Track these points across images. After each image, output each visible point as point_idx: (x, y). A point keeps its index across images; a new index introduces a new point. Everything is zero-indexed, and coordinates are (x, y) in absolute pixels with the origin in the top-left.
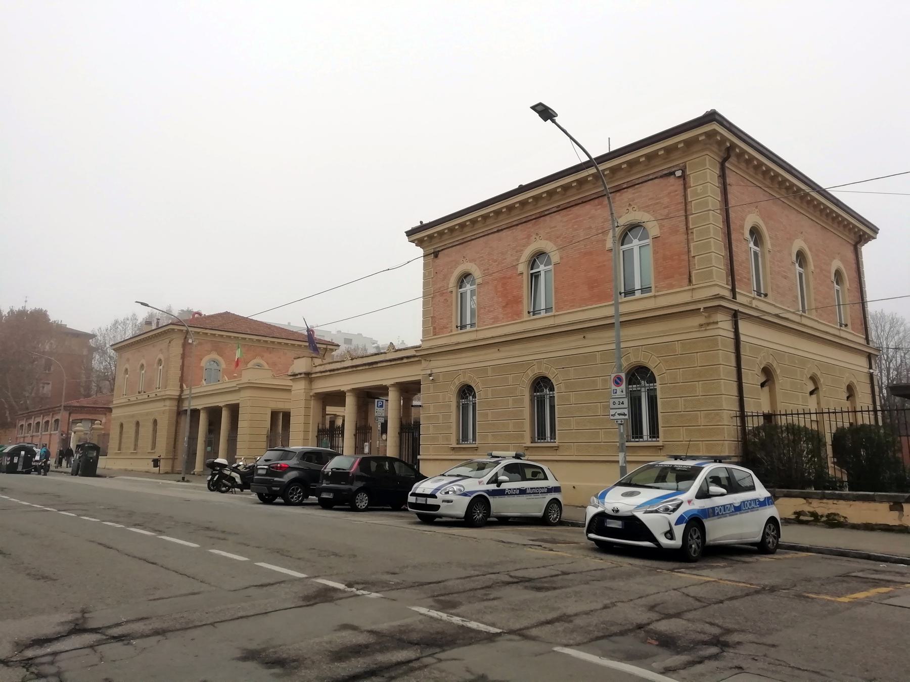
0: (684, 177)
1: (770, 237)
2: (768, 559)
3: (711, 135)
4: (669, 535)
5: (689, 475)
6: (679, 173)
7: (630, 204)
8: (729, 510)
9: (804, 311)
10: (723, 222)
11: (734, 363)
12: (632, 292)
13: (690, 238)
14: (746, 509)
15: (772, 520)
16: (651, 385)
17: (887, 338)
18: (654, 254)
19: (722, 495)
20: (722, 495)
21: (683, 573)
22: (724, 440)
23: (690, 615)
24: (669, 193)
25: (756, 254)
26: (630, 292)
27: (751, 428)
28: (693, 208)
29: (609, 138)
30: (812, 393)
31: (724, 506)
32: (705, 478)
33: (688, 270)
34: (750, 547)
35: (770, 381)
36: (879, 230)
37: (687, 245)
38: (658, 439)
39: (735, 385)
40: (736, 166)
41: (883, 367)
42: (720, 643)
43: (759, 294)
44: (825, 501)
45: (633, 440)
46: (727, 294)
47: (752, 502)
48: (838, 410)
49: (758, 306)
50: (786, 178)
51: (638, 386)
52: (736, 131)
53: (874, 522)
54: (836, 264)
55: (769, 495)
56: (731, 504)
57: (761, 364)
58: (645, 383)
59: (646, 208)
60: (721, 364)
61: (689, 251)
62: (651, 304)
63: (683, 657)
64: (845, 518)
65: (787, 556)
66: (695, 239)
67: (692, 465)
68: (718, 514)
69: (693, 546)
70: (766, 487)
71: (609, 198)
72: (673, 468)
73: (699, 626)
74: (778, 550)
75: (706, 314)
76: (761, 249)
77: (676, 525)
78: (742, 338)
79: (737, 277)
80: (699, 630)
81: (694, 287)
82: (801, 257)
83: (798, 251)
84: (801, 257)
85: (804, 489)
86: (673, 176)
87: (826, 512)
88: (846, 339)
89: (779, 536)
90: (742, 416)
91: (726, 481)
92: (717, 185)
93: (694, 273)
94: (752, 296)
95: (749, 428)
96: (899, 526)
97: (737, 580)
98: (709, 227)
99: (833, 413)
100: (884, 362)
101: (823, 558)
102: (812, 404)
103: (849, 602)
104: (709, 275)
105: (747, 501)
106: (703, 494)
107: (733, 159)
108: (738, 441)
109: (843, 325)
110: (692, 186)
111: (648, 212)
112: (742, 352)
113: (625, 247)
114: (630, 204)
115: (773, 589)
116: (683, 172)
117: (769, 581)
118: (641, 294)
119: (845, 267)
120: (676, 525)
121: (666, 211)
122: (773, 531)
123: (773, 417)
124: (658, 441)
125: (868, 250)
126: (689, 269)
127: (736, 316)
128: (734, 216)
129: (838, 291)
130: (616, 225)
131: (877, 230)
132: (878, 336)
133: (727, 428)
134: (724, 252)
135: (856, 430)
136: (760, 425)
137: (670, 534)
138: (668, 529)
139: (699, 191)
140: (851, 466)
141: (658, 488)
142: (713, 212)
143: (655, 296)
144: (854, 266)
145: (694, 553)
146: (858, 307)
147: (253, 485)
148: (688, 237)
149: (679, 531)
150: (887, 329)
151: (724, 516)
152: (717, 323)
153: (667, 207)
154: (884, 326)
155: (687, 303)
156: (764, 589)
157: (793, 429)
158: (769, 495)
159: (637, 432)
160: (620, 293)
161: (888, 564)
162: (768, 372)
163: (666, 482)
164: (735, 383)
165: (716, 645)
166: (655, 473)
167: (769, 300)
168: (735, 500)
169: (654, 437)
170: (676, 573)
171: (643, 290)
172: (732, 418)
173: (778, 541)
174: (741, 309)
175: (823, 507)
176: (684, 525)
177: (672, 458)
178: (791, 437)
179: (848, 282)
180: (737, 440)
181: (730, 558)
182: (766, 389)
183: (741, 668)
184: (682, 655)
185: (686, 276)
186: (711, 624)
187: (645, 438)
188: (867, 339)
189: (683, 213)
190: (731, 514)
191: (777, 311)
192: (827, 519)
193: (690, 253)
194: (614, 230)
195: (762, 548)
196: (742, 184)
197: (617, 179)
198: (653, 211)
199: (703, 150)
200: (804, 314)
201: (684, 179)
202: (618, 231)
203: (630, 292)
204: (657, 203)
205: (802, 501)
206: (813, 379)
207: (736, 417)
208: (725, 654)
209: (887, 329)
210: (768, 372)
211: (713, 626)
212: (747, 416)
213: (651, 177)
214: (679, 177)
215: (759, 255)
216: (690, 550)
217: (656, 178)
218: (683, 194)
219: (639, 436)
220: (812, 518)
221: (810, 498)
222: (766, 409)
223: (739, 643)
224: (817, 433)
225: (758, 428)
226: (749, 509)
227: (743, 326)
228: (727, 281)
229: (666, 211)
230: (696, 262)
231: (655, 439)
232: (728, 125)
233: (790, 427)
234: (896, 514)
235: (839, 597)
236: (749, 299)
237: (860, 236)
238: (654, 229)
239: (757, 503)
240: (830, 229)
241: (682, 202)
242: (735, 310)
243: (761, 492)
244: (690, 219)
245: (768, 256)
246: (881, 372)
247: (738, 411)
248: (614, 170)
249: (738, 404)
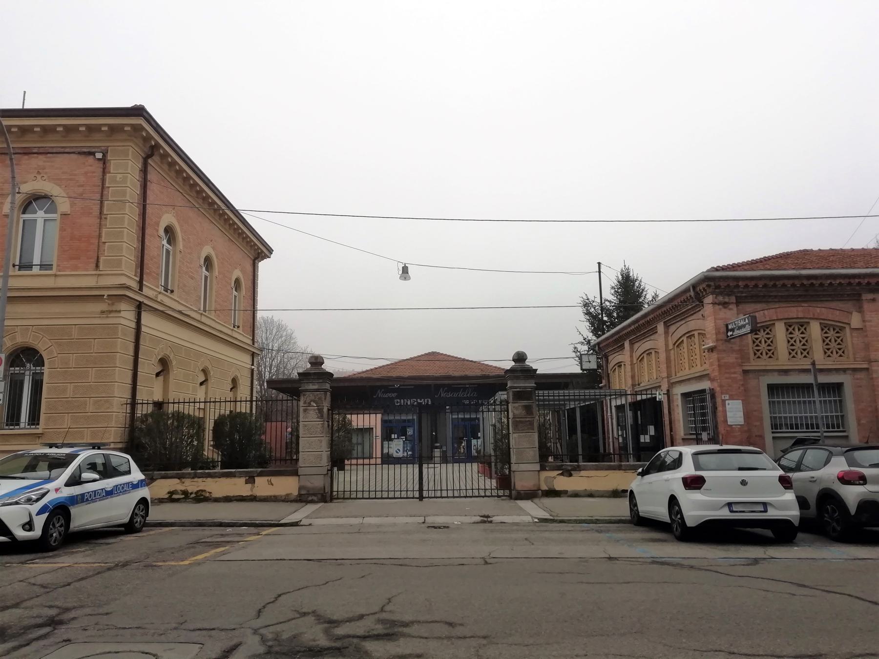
0: (104, 160)
1: (183, 239)
2: (132, 538)
3: (137, 129)
4: (27, 526)
5: (61, 463)
6: (99, 156)
7: (38, 171)
8: (100, 495)
9: (205, 311)
10: (139, 215)
11: (132, 352)
12: (29, 267)
13: (103, 223)
14: (118, 493)
15: (143, 501)
16: (37, 368)
17: (273, 340)
18: (60, 230)
19: (94, 480)
20: (94, 480)
21: (37, 563)
22: (107, 427)
23: (29, 604)
24: (86, 173)
25: (168, 252)
26: (25, 266)
27: (140, 415)
28: (110, 193)
29: (25, 92)
30: (201, 384)
31: (95, 491)
32: (79, 465)
33: (96, 255)
34: (111, 529)
35: (165, 372)
36: (273, 251)
37: (98, 230)
38: (37, 426)
39: (130, 374)
40: (159, 165)
41: (267, 364)
42: (54, 623)
43: (166, 290)
44: (196, 480)
45: (7, 427)
46: (134, 285)
47: (125, 485)
48: (223, 399)
49: (164, 301)
50: (203, 189)
51: (22, 368)
52: (162, 133)
53: (232, 495)
54: (237, 273)
55: (143, 477)
56: (102, 489)
57: (158, 354)
58: (30, 367)
59: (57, 181)
60: (118, 352)
61: (100, 236)
62: (49, 283)
63: (9, 644)
64: (210, 493)
65: (151, 533)
66: (108, 225)
67: (67, 453)
68: (87, 500)
69: (54, 535)
70: (141, 471)
71: (11, 159)
72: (45, 456)
73: (35, 612)
74: (144, 529)
75: (110, 302)
76: (173, 248)
77: (36, 515)
78: (143, 329)
79: (146, 271)
80: (35, 615)
81: (101, 272)
82: (208, 262)
83: (206, 257)
84: (208, 262)
85: (181, 471)
86: (92, 156)
87: (195, 489)
88: (236, 339)
89: (147, 514)
90: (133, 404)
91: (102, 466)
92: (138, 179)
93: (102, 259)
94: (159, 290)
95: (138, 415)
96: (251, 496)
97: (93, 561)
98: (124, 217)
99: (213, 402)
100: (268, 360)
101: (183, 530)
102: (200, 395)
103: (190, 564)
104: (119, 264)
105: (121, 485)
106: (74, 481)
107: (156, 158)
108: (125, 428)
109: (236, 327)
110: (111, 172)
111: (60, 186)
112: (142, 342)
113: (27, 216)
114: (38, 171)
115: (125, 564)
116: (104, 155)
117: (123, 558)
118: (40, 270)
119: (244, 277)
120: (36, 515)
121: (81, 190)
122: (142, 512)
123: (165, 405)
124: (38, 428)
125: (262, 265)
126: (98, 254)
127: (140, 307)
128: (151, 212)
129: (235, 296)
130: (17, 191)
131: (271, 251)
132: (267, 338)
133: (116, 415)
134: (136, 244)
135: (234, 417)
136: (149, 412)
137: (29, 526)
138: (27, 520)
139: (118, 179)
140: (225, 448)
141: (23, 478)
142: (131, 204)
143: (56, 276)
144: (251, 277)
145: (55, 542)
146: (250, 313)
147: (650, 374)
148: (100, 221)
149: (39, 522)
150: (274, 332)
151: (93, 501)
152: (120, 311)
153: (82, 186)
154: (272, 330)
155: (91, 288)
156: (117, 565)
157: (179, 417)
158: (143, 477)
159: (13, 418)
160: (14, 266)
161: (235, 528)
162: (164, 363)
163: (36, 471)
164: (131, 371)
165: (49, 625)
166: (25, 462)
167: (175, 296)
168: (108, 484)
169: (33, 424)
170: (27, 565)
171: (42, 266)
172: (122, 405)
173: (145, 520)
174: (146, 302)
175: (192, 486)
176: (46, 515)
177: (45, 446)
178: (176, 424)
179: (244, 292)
180: (124, 426)
181: (94, 541)
182: (161, 378)
183: (69, 640)
184: (9, 643)
185: (94, 260)
186: (50, 607)
187: (22, 425)
188: (253, 340)
189: (98, 196)
190: (102, 498)
191: (180, 308)
192: (195, 495)
193: (101, 238)
194: (14, 195)
195: (129, 528)
196: (163, 184)
197: (27, 141)
198: (66, 187)
199: (126, 140)
200: (204, 313)
201: (104, 163)
202: (19, 198)
203: (25, 266)
204: (71, 180)
205: (177, 481)
206: (205, 371)
207: (127, 404)
208: (56, 631)
209: (274, 332)
210: (164, 363)
211: (52, 609)
212: (137, 404)
213: (67, 150)
214: (99, 159)
215: (171, 253)
216: (50, 539)
217: (74, 153)
218: (101, 177)
219: (36, 422)
220: (183, 496)
221: (184, 478)
222: (158, 397)
223: (74, 619)
224: (198, 420)
225: (146, 415)
226: (121, 492)
227: (147, 319)
228: (136, 272)
229: (81, 190)
230: (106, 248)
231: (34, 427)
232: (155, 125)
233: (176, 415)
234: (249, 486)
235: (182, 561)
236: (155, 293)
237: (259, 253)
238: (64, 206)
239: (130, 486)
240: (236, 242)
241: (99, 186)
242: (140, 302)
243: (137, 475)
244: (105, 205)
245: (178, 256)
246: (265, 368)
247: (129, 399)
248: (24, 131)
249: (130, 391)
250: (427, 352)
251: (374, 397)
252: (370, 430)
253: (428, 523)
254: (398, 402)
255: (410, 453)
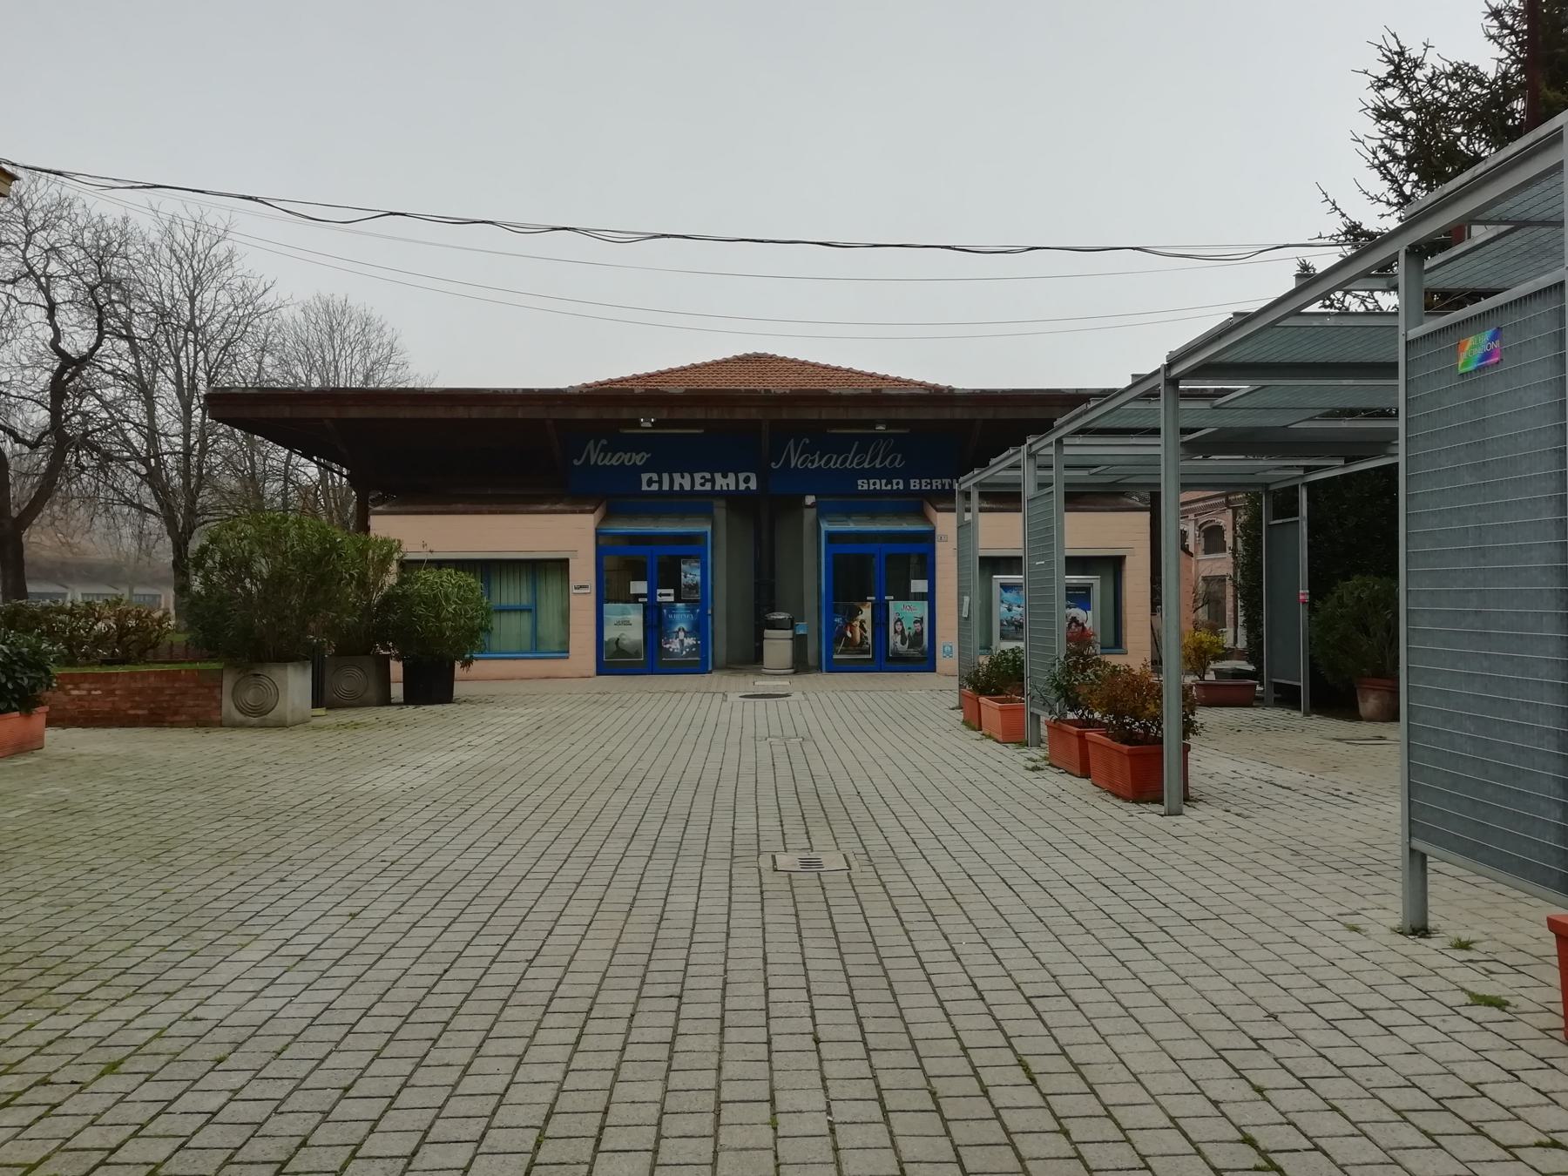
250: (740, 353)
251: (576, 462)
252: (561, 566)
253: (1188, 728)
254: (648, 482)
255: (690, 641)
